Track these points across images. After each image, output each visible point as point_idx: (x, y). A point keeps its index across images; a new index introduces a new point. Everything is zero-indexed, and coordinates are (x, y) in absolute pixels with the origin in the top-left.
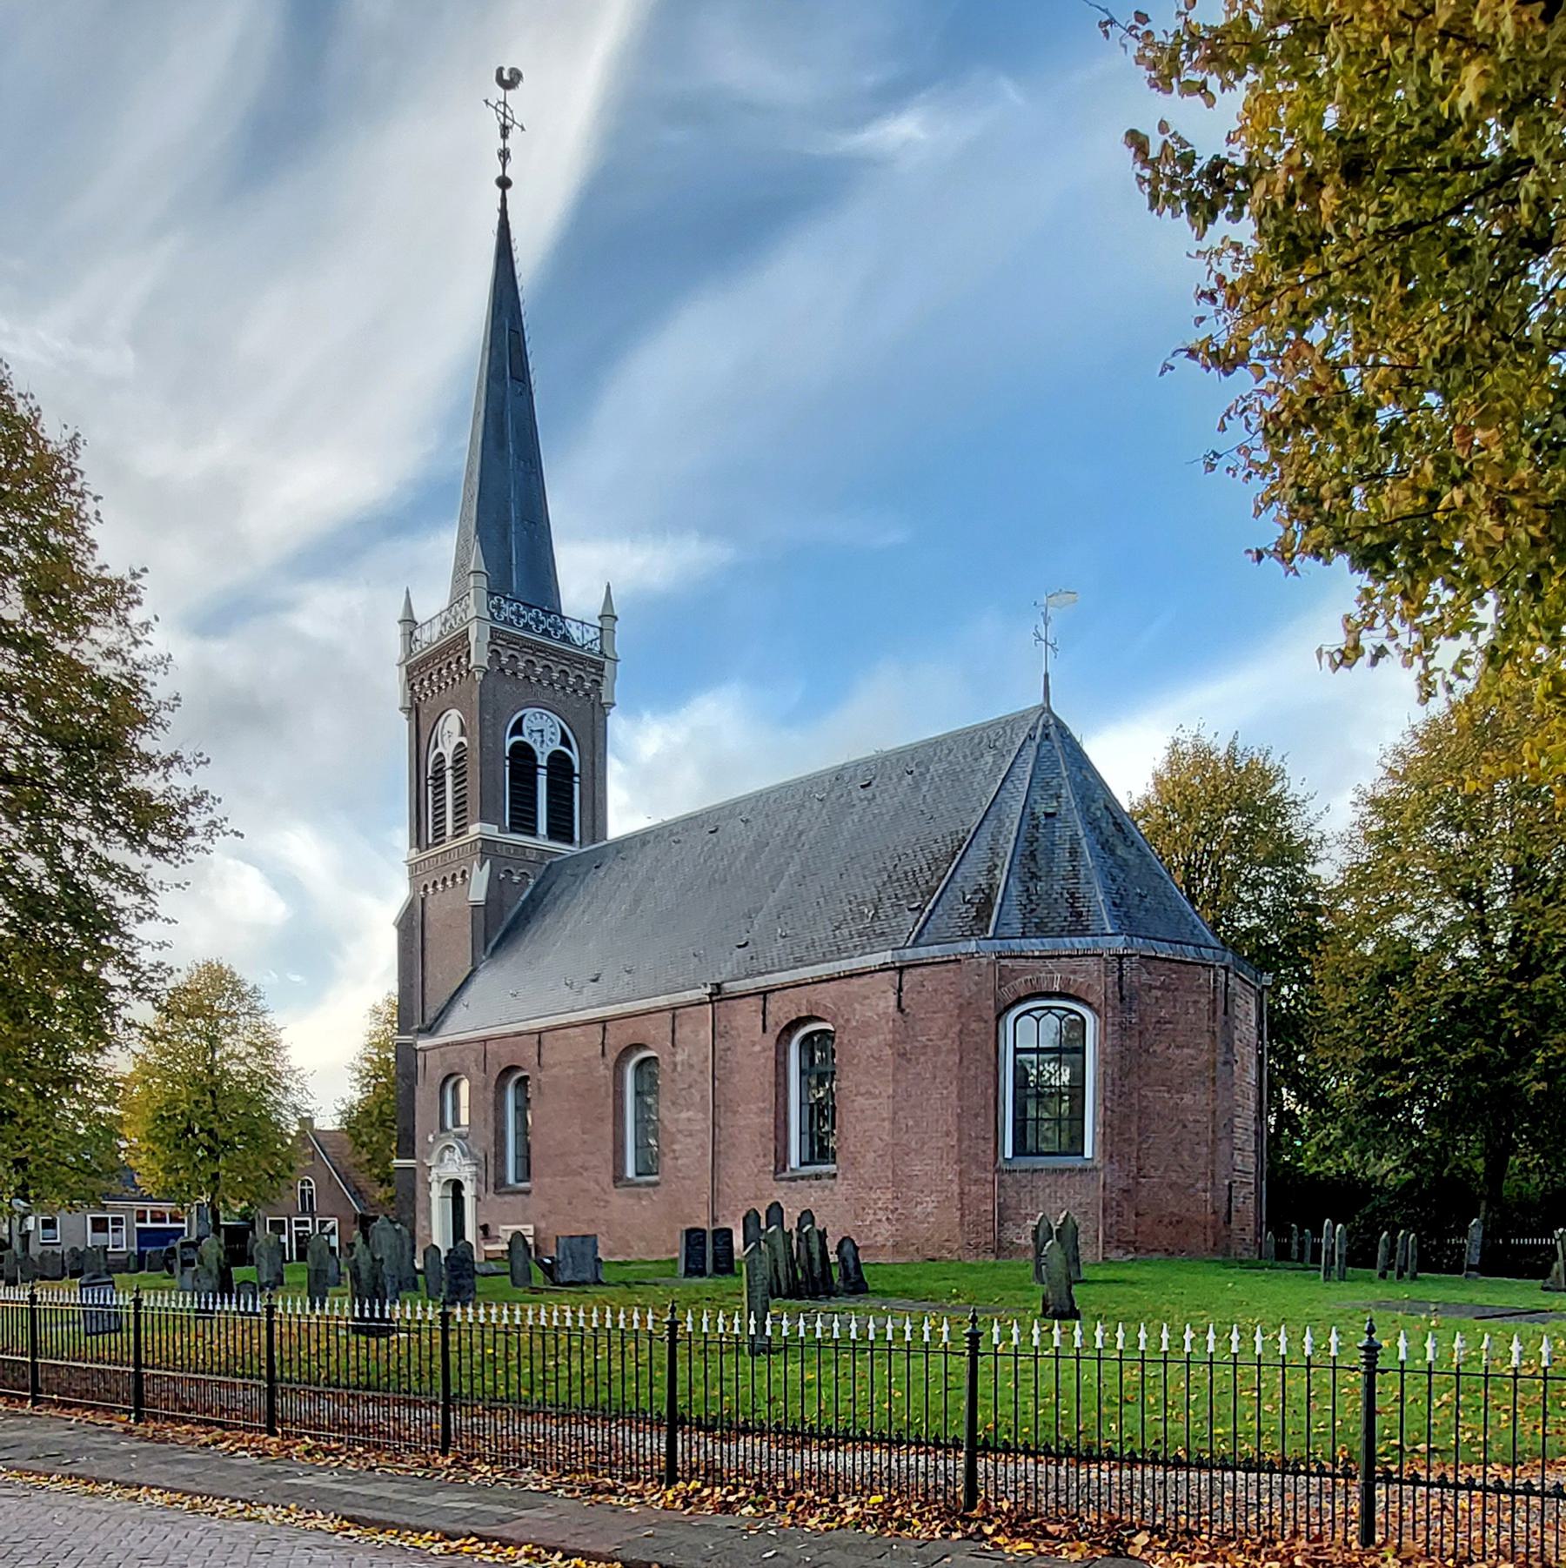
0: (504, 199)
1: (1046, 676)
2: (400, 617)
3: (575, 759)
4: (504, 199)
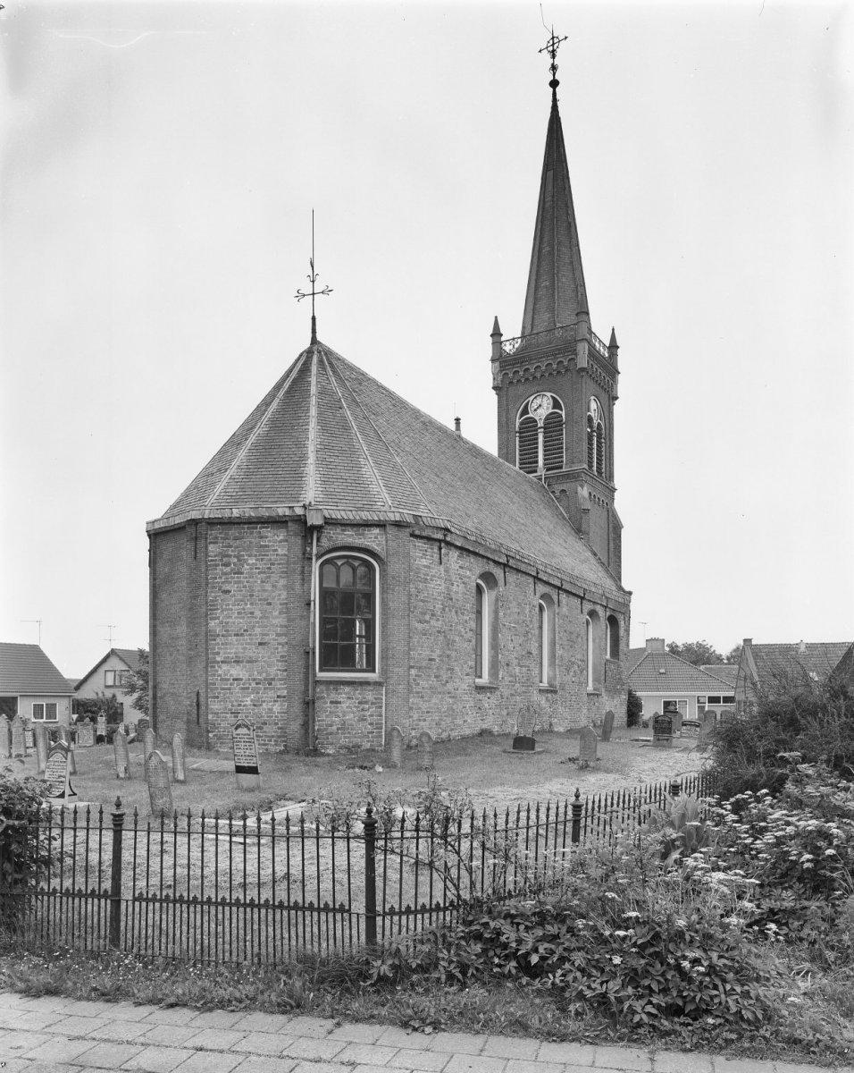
0: (554, 94)
1: (314, 319)
2: (491, 332)
3: (563, 414)
4: (554, 94)
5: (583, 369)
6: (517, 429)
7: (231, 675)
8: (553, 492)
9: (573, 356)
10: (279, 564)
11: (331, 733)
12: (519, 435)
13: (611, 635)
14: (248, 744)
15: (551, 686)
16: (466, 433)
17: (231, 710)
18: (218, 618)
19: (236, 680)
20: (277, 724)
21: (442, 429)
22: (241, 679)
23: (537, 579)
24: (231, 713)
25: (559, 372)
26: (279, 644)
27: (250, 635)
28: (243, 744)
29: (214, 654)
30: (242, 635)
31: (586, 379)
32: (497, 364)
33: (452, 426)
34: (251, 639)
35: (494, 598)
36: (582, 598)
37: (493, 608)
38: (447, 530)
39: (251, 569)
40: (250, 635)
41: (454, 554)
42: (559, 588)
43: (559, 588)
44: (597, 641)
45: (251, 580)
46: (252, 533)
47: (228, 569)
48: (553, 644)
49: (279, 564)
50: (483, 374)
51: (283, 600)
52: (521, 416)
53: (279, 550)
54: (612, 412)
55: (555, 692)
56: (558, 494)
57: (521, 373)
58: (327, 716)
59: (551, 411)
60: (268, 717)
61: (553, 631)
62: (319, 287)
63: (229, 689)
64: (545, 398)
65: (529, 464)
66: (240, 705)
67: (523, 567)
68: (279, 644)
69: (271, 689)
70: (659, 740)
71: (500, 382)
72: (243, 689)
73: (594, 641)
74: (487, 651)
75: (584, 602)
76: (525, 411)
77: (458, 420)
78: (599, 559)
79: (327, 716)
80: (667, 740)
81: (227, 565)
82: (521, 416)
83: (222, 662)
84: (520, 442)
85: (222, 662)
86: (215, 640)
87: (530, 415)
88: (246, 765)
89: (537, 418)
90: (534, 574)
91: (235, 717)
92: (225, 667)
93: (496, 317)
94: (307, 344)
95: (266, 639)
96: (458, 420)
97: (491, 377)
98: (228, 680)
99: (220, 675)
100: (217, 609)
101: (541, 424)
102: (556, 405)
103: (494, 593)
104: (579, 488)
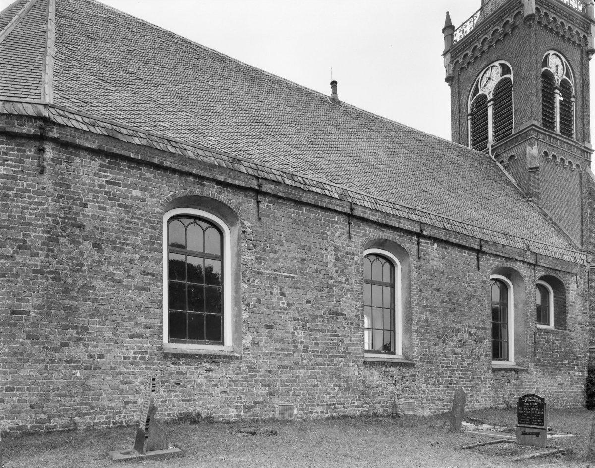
5: (531, 17)
6: (469, 112)
8: (502, 162)
9: (519, 10)
12: (471, 116)
13: (555, 301)
15: (406, 358)
16: (342, 97)
21: (322, 100)
23: (350, 217)
25: (506, 35)
31: (535, 28)
32: (448, 56)
33: (327, 92)
35: (236, 237)
36: (479, 252)
37: (235, 250)
38: (46, 120)
41: (435, 249)
42: (420, 235)
43: (420, 235)
44: (520, 306)
48: (408, 305)
50: (437, 67)
54: (587, 69)
55: (411, 366)
56: (506, 161)
59: (500, 79)
61: (408, 289)
64: (495, 69)
65: (480, 140)
67: (306, 198)
70: (524, 433)
71: (451, 72)
73: (515, 306)
74: (399, 330)
75: (537, 268)
76: (477, 90)
77: (334, 84)
78: (551, 219)
80: (537, 434)
84: (472, 123)
87: (481, 92)
89: (487, 93)
90: (347, 211)
93: (448, 13)
95: (23, 306)
96: (334, 84)
97: (444, 70)
103: (237, 229)
104: (528, 148)
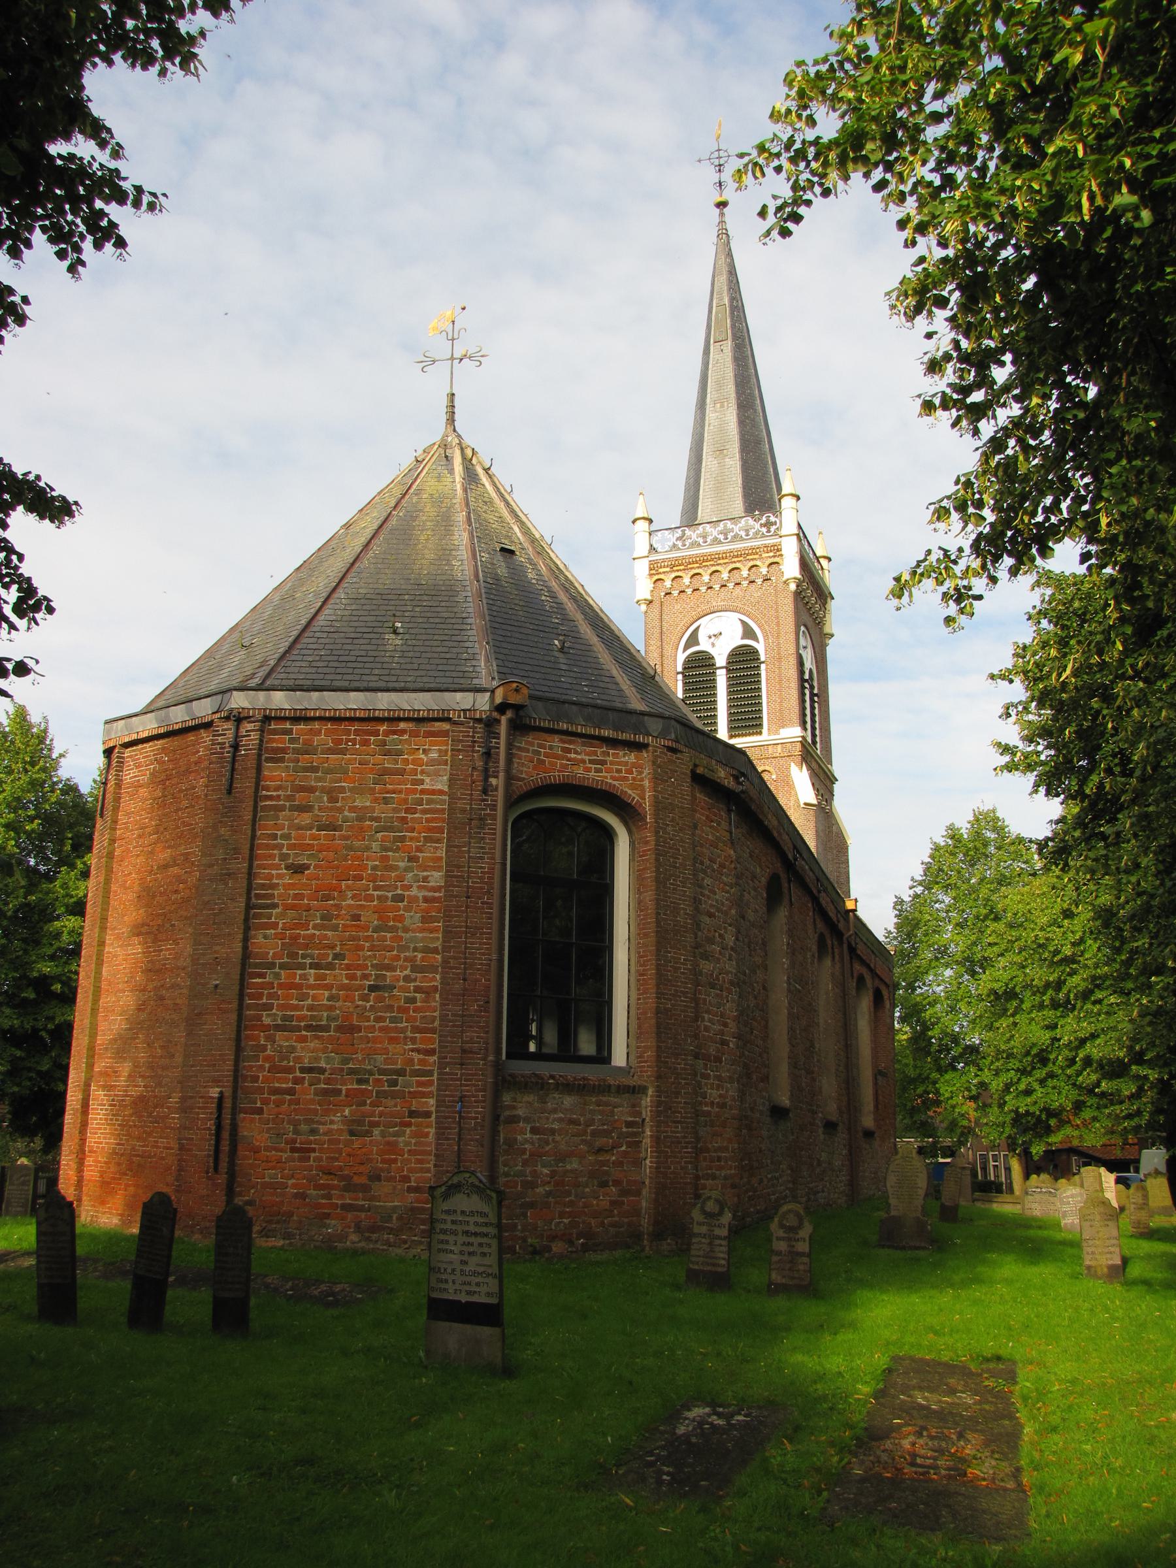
7: (298, 1059)
9: (776, 560)
10: (424, 812)
11: (532, 1205)
14: (476, 1240)
17: (294, 1141)
18: (275, 926)
19: (310, 1070)
20: (406, 1179)
22: (322, 1071)
24: (293, 1150)
26: (417, 989)
27: (348, 967)
28: (462, 1239)
29: (257, 1007)
30: (330, 966)
34: (352, 977)
39: (360, 819)
40: (348, 967)
45: (357, 843)
46: (366, 743)
47: (306, 819)
49: (424, 812)
51: (433, 889)
52: (684, 650)
53: (427, 780)
57: (668, 584)
58: (525, 1163)
60: (384, 1161)
62: (442, 349)
63: (291, 1092)
66: (313, 1132)
68: (417, 989)
69: (394, 1095)
72: (325, 1092)
76: (693, 640)
79: (525, 1163)
81: (305, 809)
82: (684, 650)
83: (278, 1028)
85: (278, 1028)
86: (262, 976)
88: (464, 1298)
91: (301, 1159)
92: (283, 1040)
94: (436, 430)
98: (290, 1070)
99: (267, 1059)
100: (275, 906)
101: (721, 660)
102: (748, 633)
